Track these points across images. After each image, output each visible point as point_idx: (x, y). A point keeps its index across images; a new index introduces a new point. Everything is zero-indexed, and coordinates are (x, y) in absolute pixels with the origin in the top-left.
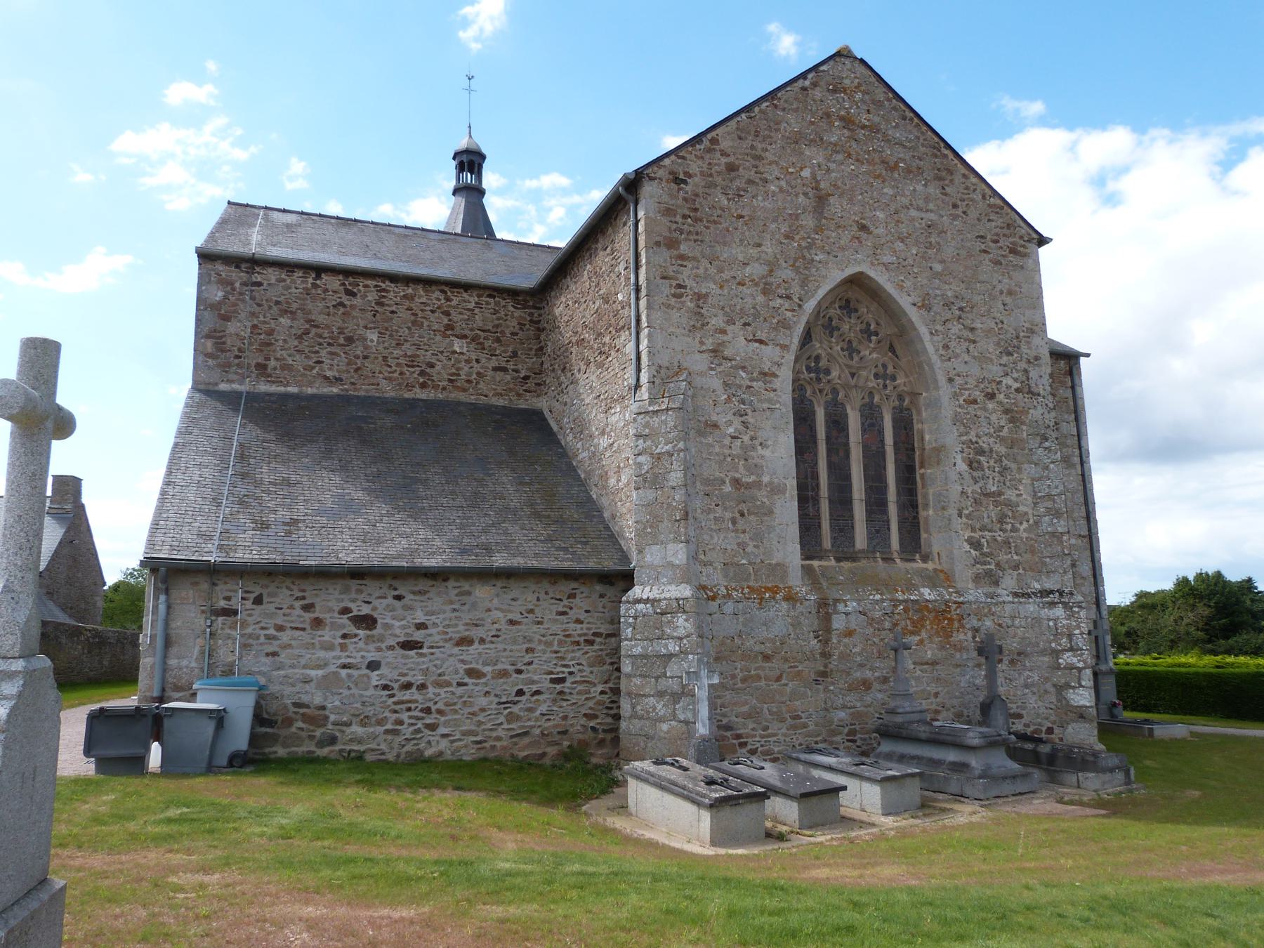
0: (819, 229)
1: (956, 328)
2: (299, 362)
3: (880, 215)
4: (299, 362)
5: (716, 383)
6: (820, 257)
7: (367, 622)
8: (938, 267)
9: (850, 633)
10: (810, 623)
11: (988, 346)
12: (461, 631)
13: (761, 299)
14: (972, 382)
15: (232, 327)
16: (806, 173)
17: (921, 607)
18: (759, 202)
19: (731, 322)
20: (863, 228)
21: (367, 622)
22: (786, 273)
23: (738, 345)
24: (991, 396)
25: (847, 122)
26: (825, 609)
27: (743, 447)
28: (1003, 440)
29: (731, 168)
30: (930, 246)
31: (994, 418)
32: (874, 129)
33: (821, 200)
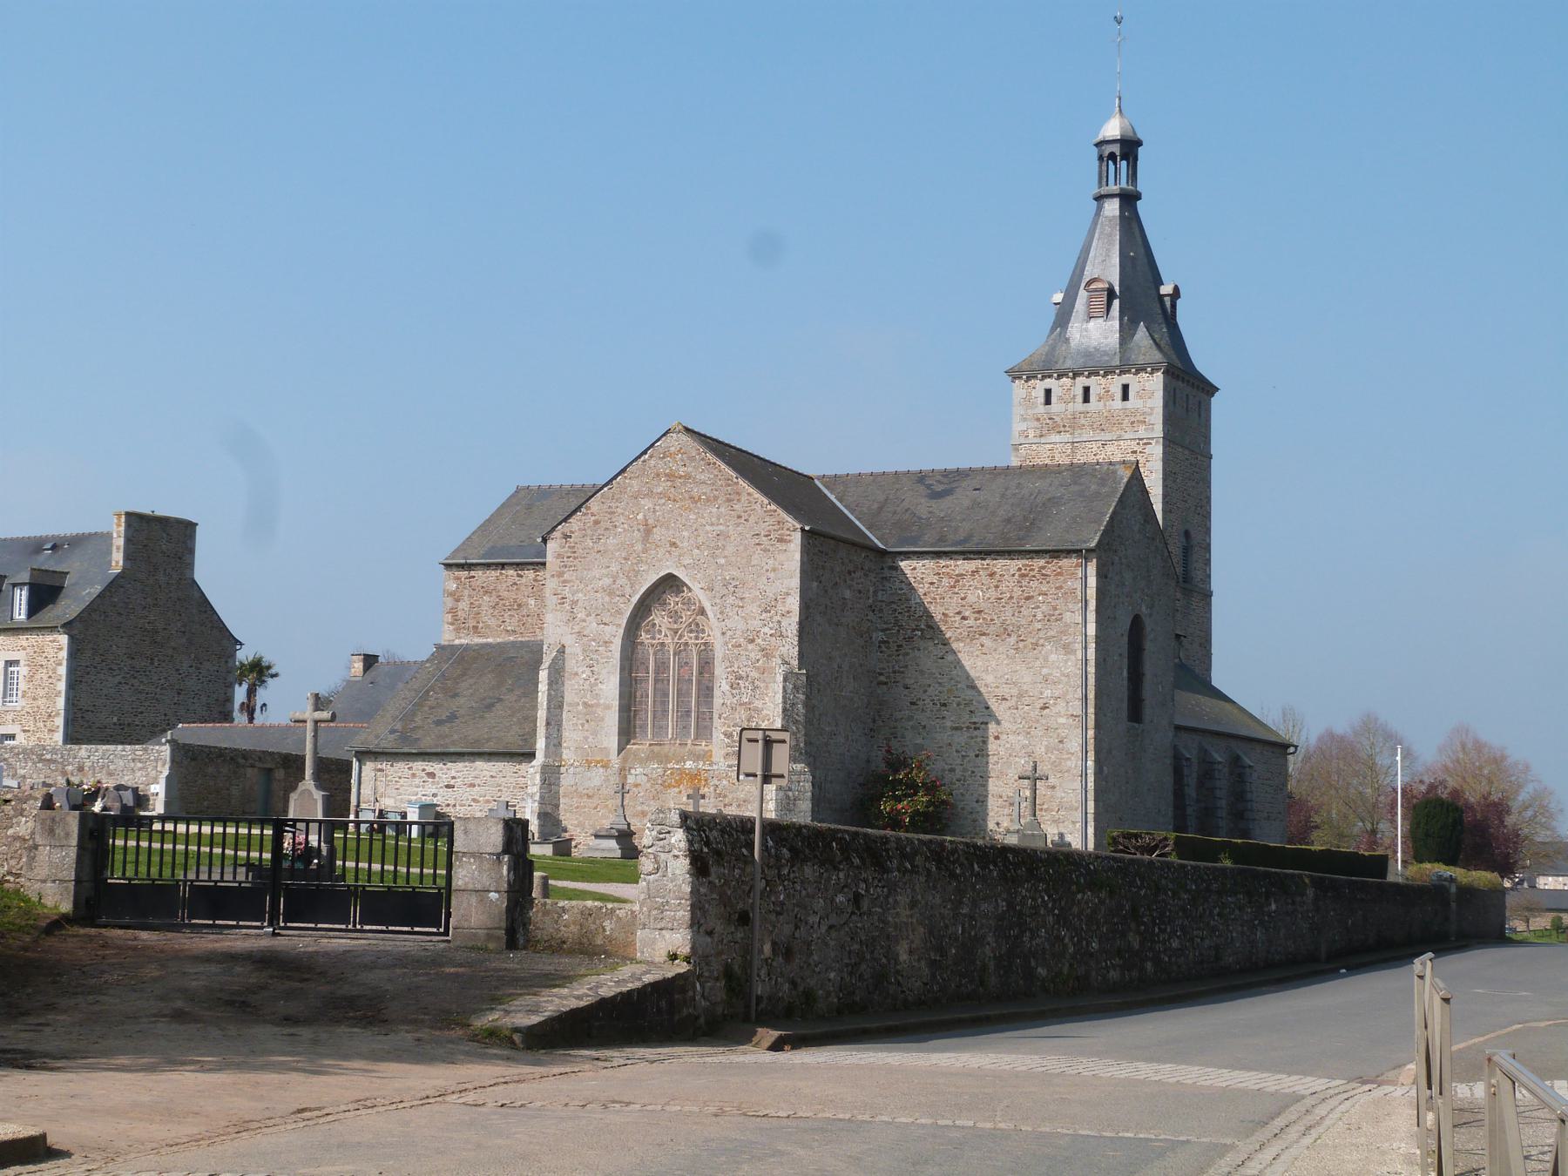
0: (645, 551)
1: (731, 600)
2: (492, 622)
3: (685, 534)
4: (492, 622)
5: (579, 650)
6: (645, 567)
7: (432, 775)
8: (722, 561)
9: (637, 786)
10: (615, 779)
11: (754, 609)
12: (470, 780)
13: (607, 599)
14: (739, 633)
15: (462, 605)
16: (640, 517)
17: (682, 772)
18: (611, 541)
19: (589, 615)
20: (674, 544)
21: (432, 775)
22: (622, 581)
23: (592, 626)
24: (752, 641)
25: (671, 476)
26: (623, 772)
27: (592, 686)
28: (757, 669)
29: (597, 522)
30: (718, 548)
31: (752, 655)
32: (688, 476)
33: (648, 531)
